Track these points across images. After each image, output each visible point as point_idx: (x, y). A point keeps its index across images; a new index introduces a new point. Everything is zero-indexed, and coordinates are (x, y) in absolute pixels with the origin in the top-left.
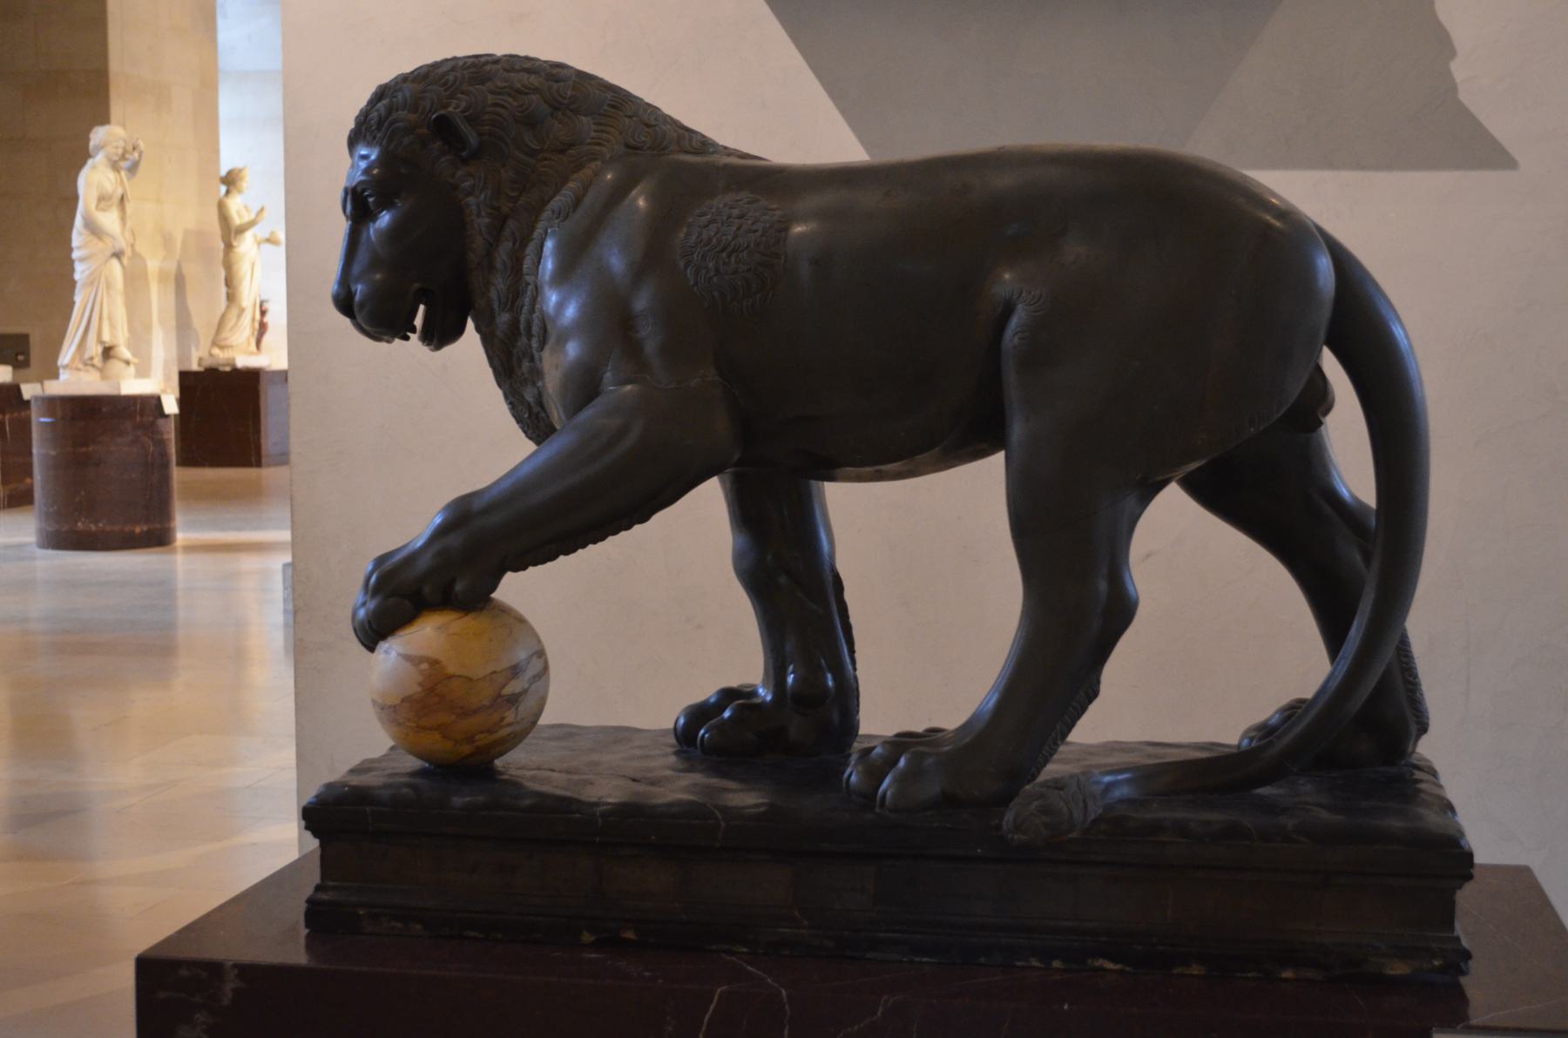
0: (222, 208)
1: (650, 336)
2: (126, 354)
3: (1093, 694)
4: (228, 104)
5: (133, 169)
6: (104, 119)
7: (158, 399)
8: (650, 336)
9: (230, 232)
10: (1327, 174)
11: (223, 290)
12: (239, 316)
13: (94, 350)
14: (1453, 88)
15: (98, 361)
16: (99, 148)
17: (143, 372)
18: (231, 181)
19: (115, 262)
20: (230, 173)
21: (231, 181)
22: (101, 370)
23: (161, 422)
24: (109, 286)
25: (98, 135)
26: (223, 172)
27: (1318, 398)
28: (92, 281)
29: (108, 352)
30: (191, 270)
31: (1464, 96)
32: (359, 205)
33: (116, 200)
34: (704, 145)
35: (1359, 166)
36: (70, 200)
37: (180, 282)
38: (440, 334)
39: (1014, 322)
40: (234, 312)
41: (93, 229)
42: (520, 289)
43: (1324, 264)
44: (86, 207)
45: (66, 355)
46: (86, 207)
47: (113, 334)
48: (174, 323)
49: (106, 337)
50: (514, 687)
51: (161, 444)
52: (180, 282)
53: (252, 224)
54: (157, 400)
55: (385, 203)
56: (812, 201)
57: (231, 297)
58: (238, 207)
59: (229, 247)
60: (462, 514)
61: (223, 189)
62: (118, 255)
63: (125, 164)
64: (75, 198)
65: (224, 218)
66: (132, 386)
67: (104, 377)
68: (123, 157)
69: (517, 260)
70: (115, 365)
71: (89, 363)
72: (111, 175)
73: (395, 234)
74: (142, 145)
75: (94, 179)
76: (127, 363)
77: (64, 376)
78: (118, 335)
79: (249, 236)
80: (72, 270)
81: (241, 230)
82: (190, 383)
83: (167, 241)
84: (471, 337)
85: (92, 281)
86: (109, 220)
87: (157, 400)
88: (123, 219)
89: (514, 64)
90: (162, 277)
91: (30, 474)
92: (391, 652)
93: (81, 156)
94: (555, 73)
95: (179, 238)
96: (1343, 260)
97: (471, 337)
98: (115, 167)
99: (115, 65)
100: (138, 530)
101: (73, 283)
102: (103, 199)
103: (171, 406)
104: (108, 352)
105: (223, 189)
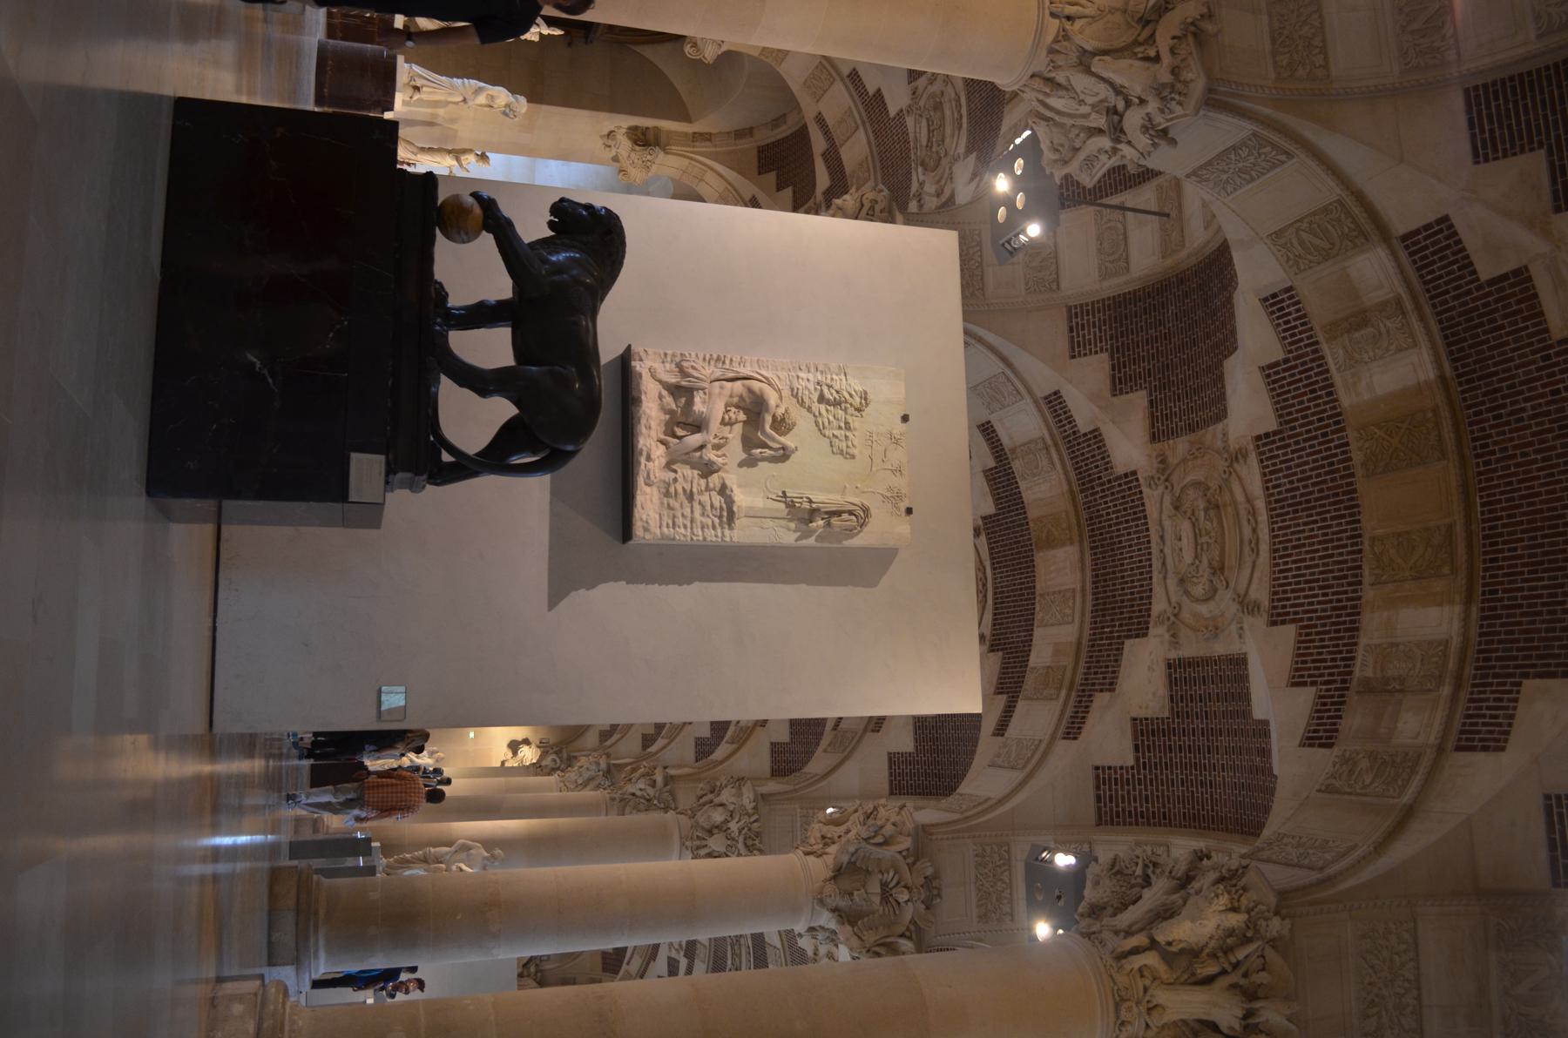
0: (470, 151)
1: (557, 278)
2: (415, 98)
3: (461, 386)
4: (518, 161)
5: (505, 113)
6: (528, 102)
7: (392, 110)
8: (557, 278)
9: (457, 153)
10: (547, 548)
11: (427, 146)
12: (412, 152)
13: (419, 83)
14: (576, 590)
15: (413, 83)
16: (516, 99)
17: (405, 103)
18: (483, 157)
19: (461, 99)
20: (487, 157)
21: (483, 157)
22: (408, 84)
23: (380, 110)
24: (450, 94)
25: (523, 100)
26: (488, 154)
27: (534, 453)
28: (452, 86)
29: (417, 89)
30: (436, 131)
31: (573, 594)
32: (589, 207)
33: (491, 104)
34: (602, 300)
35: (550, 558)
36: (494, 82)
37: (431, 124)
38: (551, 225)
39: (561, 369)
40: (415, 150)
41: (478, 91)
42: (567, 248)
43: (570, 448)
44: (489, 89)
45: (416, 68)
46: (489, 89)
47: (425, 92)
48: (409, 118)
49: (424, 89)
50: (462, 233)
51: (369, 109)
52: (431, 124)
53: (461, 165)
54: (391, 109)
55: (589, 214)
56: (590, 325)
57: (422, 149)
58: (470, 159)
59: (449, 152)
60: (509, 223)
61: (479, 153)
62: (465, 100)
63: (508, 111)
64: (494, 85)
65: (465, 151)
66: (399, 98)
67: (405, 85)
68: (511, 110)
69: (574, 247)
70: (410, 91)
71: (412, 79)
72: (503, 103)
73: (581, 215)
74: (516, 119)
75: (502, 95)
76: (411, 98)
77: (406, 66)
78: (425, 95)
79: (455, 163)
80: (458, 78)
81: (458, 159)
82: (394, 125)
83: (453, 121)
84: (550, 233)
85: (452, 86)
86: (482, 99)
87: (391, 109)
88: (481, 105)
89: (624, 252)
90: (434, 115)
91: (343, 39)
92: (471, 200)
93: (513, 91)
94: (621, 264)
95: (455, 127)
96: (572, 454)
97: (550, 233)
98: (507, 105)
99: (545, 108)
100: (326, 90)
101: (452, 77)
102: (492, 97)
103: (388, 115)
104: (417, 89)
105: (479, 153)
